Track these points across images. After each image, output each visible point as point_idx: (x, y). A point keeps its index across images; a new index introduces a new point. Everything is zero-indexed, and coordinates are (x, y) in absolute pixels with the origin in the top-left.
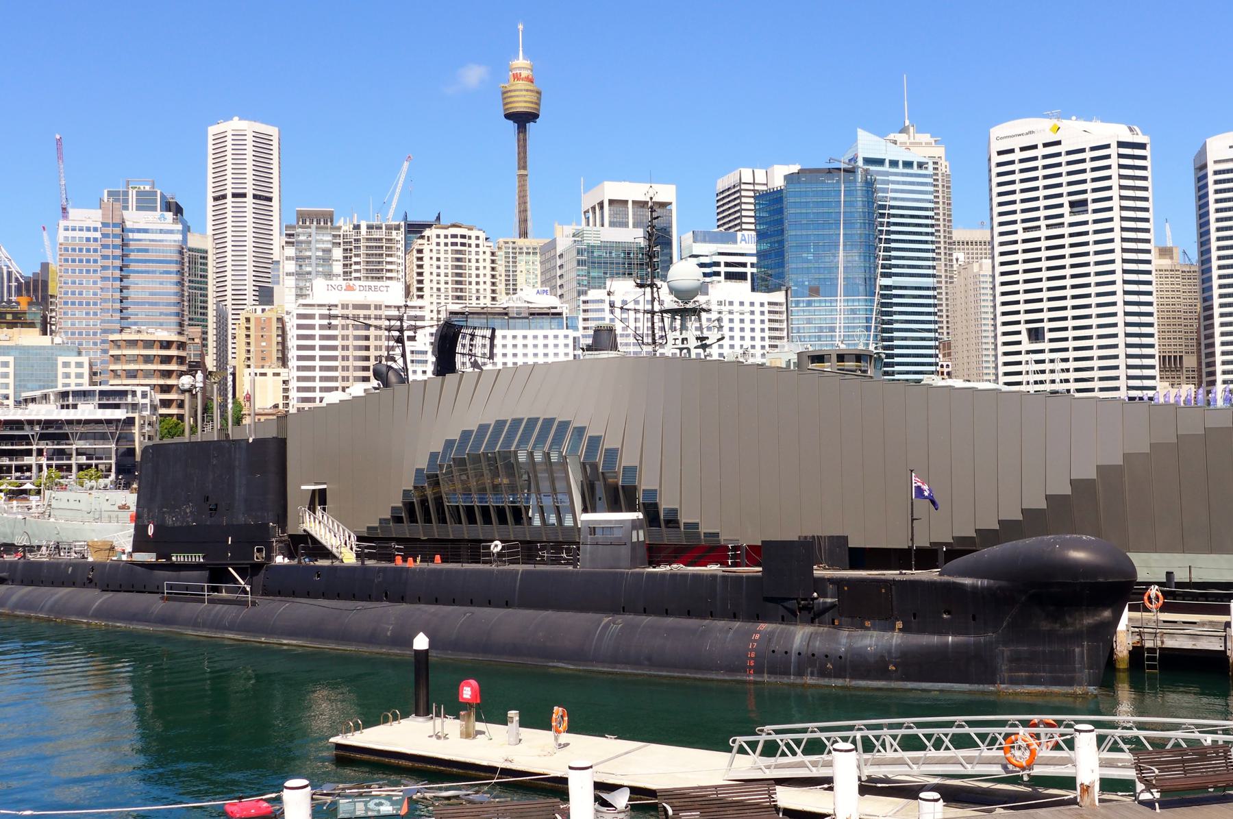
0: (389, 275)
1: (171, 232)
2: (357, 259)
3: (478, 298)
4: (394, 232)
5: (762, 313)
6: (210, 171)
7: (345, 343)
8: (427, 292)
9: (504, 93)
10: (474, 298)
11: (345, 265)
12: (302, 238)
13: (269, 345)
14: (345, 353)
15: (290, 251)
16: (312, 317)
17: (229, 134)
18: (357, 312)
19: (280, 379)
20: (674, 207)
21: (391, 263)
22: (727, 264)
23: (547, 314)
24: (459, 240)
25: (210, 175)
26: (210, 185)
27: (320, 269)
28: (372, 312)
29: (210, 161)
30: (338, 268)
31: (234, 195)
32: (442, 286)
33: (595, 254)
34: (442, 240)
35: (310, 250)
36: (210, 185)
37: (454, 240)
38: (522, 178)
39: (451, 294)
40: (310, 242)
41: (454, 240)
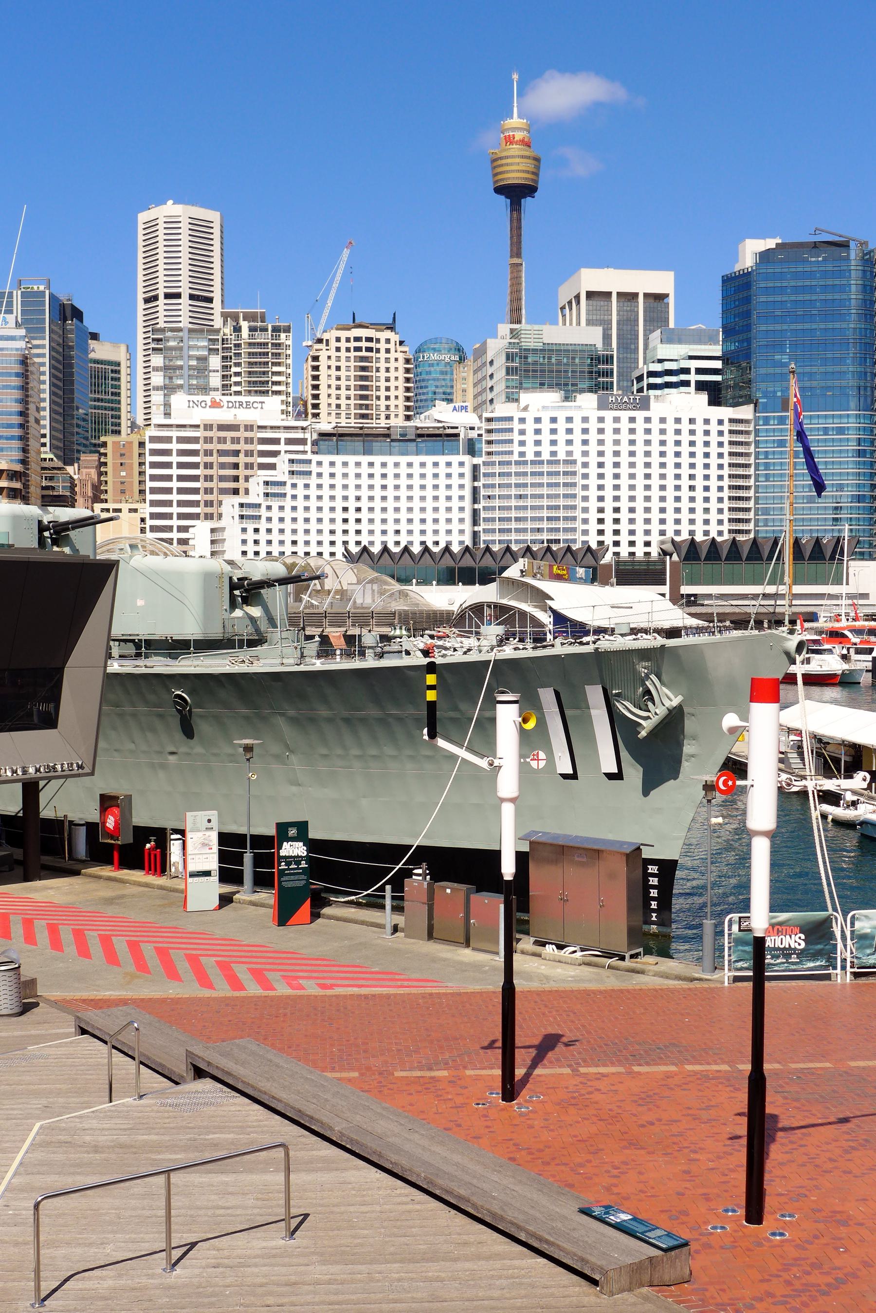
0: (275, 388)
1: (12, 338)
2: (238, 369)
3: (388, 417)
4: (283, 335)
5: (721, 433)
6: (140, 267)
7: (209, 472)
8: (323, 410)
9: (494, 161)
10: (383, 416)
11: (224, 377)
12: (172, 344)
13: (130, 475)
14: (209, 485)
15: (157, 360)
16: (168, 440)
17: (160, 222)
18: (222, 434)
19: (138, 516)
20: (671, 300)
21: (279, 373)
22: (699, 371)
23: (440, 435)
24: (364, 344)
25: (140, 273)
26: (140, 284)
27: (195, 382)
28: (242, 434)
29: (140, 255)
30: (215, 380)
31: (168, 296)
32: (343, 402)
33: (530, 360)
34: (343, 345)
35: (181, 358)
36: (140, 284)
37: (358, 344)
38: (516, 267)
39: (353, 411)
40: (181, 349)
41: (358, 344)
